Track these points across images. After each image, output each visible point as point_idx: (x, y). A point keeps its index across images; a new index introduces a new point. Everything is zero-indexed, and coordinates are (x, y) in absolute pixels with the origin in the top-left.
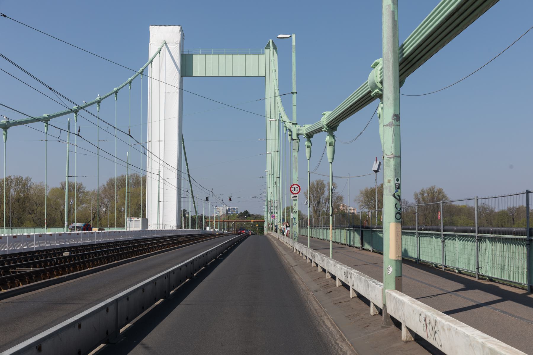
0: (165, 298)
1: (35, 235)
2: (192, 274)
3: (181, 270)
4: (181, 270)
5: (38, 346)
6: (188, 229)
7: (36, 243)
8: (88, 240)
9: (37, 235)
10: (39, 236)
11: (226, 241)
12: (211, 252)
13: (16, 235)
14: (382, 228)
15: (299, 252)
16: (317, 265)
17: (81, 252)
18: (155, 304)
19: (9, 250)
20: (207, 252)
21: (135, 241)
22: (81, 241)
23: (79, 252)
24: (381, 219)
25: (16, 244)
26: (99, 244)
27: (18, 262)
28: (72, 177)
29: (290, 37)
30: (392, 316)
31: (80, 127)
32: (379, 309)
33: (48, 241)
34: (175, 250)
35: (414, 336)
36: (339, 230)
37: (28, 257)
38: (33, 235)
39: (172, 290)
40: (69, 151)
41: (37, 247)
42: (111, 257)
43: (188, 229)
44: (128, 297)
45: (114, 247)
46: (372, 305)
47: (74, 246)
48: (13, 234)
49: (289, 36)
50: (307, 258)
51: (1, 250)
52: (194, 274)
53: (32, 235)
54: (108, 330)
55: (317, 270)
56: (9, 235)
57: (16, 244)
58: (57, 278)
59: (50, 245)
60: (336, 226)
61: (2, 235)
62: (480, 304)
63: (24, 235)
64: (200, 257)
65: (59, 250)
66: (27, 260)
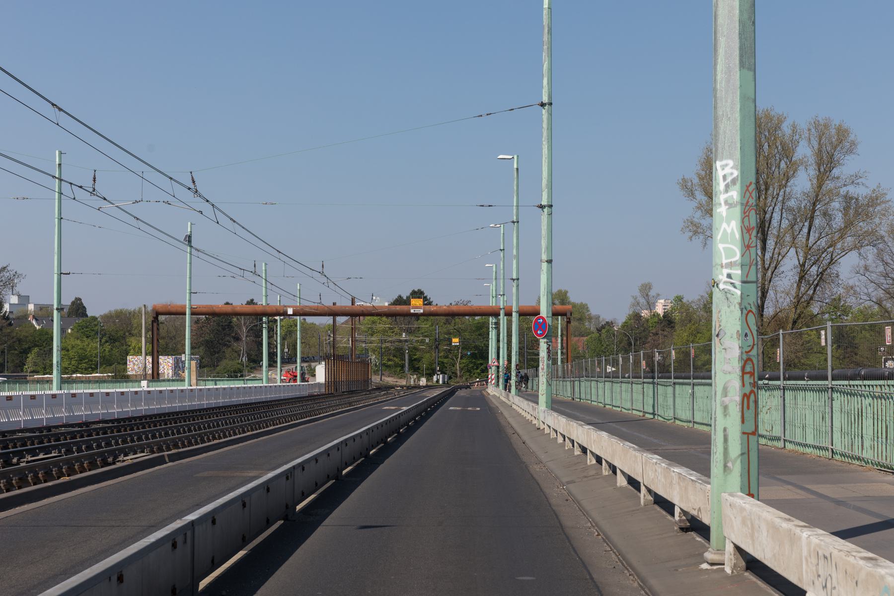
0: (286, 518)
1: (23, 395)
2: (340, 470)
3: (317, 462)
4: (317, 462)
5: (117, 574)
6: (296, 384)
7: (24, 412)
8: (154, 405)
9: (49, 394)
10: (31, 399)
11: (336, 442)
12: (344, 445)
13: (11, 394)
14: (710, 378)
15: (556, 432)
16: (614, 469)
17: (180, 422)
18: (316, 495)
19: (46, 418)
20: (369, 429)
21: (297, 400)
22: (98, 409)
23: (135, 429)
24: (778, 357)
25: (14, 411)
26: (124, 418)
27: (78, 437)
28: (69, 274)
29: (513, 158)
30: (657, 494)
31: (95, 171)
32: (627, 476)
33: (27, 410)
34: (237, 445)
35: (595, 457)
36: (778, 393)
37: (133, 424)
38: (42, 395)
39: (241, 550)
40: (62, 218)
41: (49, 417)
42: (207, 435)
43: (296, 384)
44: (215, 517)
45: (191, 419)
46: (643, 488)
47: (177, 412)
48: (15, 393)
49: (511, 157)
50: (615, 472)
51: (11, 420)
52: (388, 438)
53: (96, 393)
54: (174, 586)
55: (599, 473)
56: (24, 394)
57: (14, 411)
58: (65, 480)
59: (54, 415)
60: (835, 372)
61: (13, 394)
62: (889, 520)
63: (47, 394)
64: (381, 424)
65: (163, 417)
66: (59, 438)
